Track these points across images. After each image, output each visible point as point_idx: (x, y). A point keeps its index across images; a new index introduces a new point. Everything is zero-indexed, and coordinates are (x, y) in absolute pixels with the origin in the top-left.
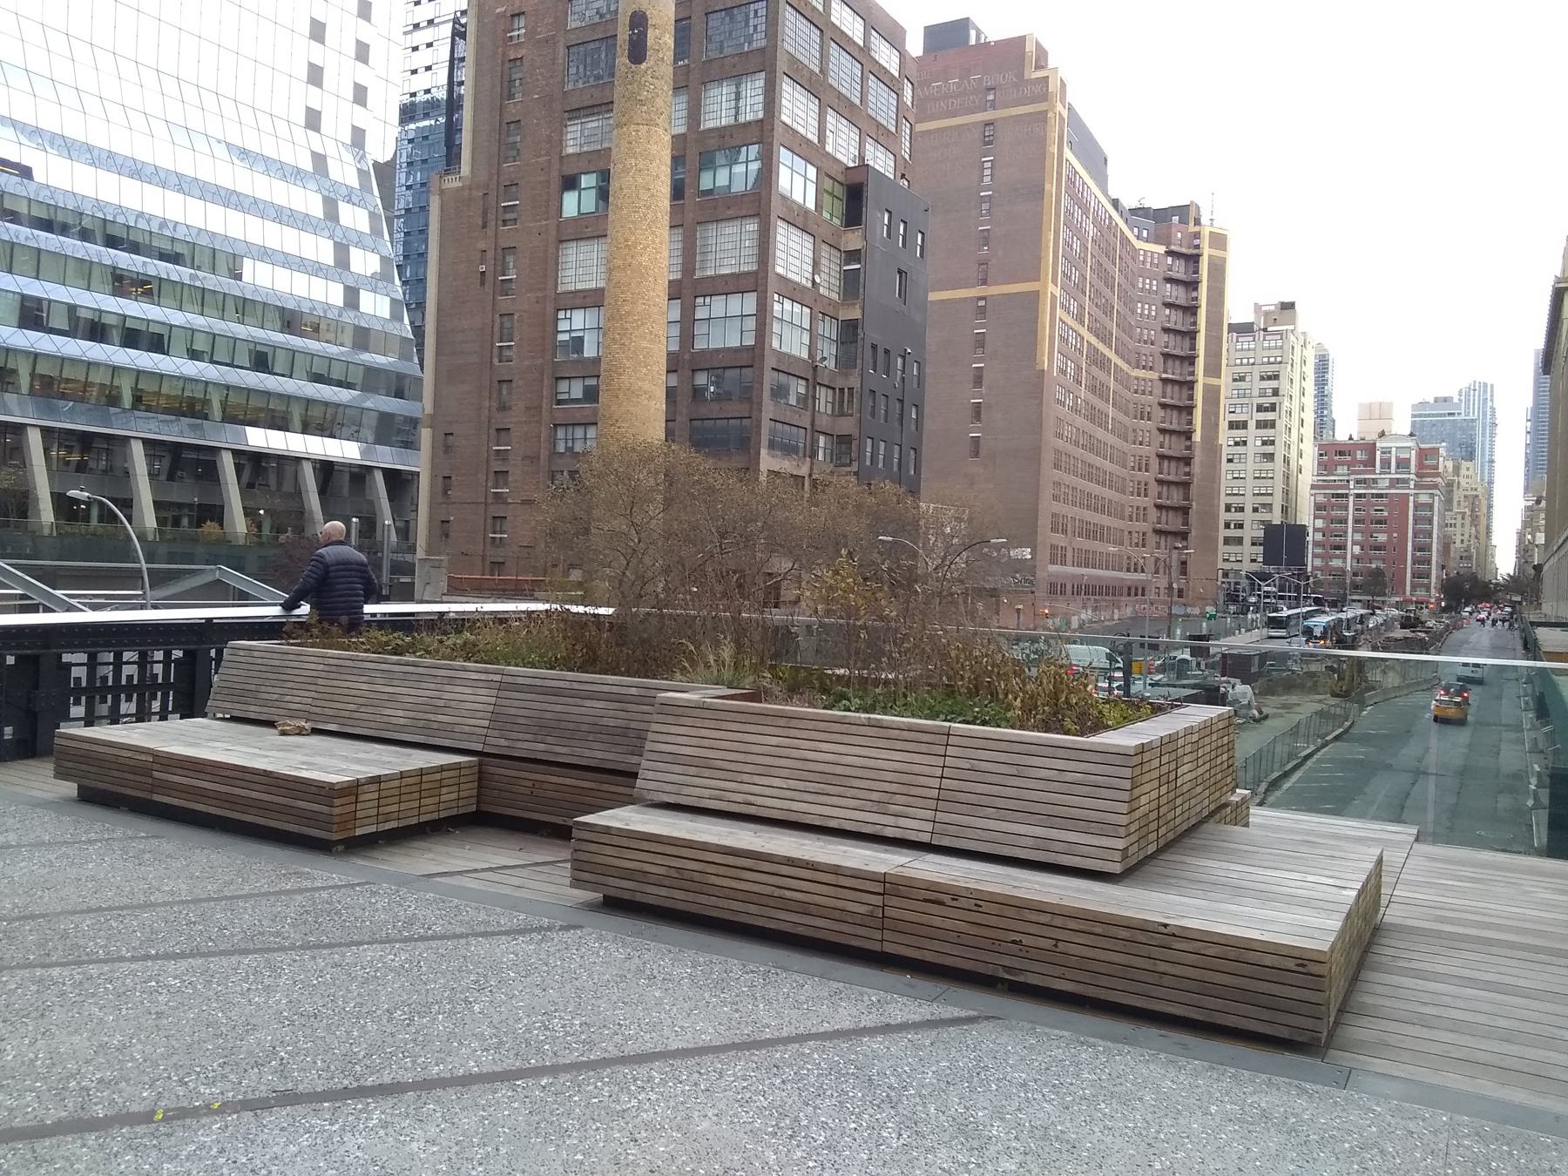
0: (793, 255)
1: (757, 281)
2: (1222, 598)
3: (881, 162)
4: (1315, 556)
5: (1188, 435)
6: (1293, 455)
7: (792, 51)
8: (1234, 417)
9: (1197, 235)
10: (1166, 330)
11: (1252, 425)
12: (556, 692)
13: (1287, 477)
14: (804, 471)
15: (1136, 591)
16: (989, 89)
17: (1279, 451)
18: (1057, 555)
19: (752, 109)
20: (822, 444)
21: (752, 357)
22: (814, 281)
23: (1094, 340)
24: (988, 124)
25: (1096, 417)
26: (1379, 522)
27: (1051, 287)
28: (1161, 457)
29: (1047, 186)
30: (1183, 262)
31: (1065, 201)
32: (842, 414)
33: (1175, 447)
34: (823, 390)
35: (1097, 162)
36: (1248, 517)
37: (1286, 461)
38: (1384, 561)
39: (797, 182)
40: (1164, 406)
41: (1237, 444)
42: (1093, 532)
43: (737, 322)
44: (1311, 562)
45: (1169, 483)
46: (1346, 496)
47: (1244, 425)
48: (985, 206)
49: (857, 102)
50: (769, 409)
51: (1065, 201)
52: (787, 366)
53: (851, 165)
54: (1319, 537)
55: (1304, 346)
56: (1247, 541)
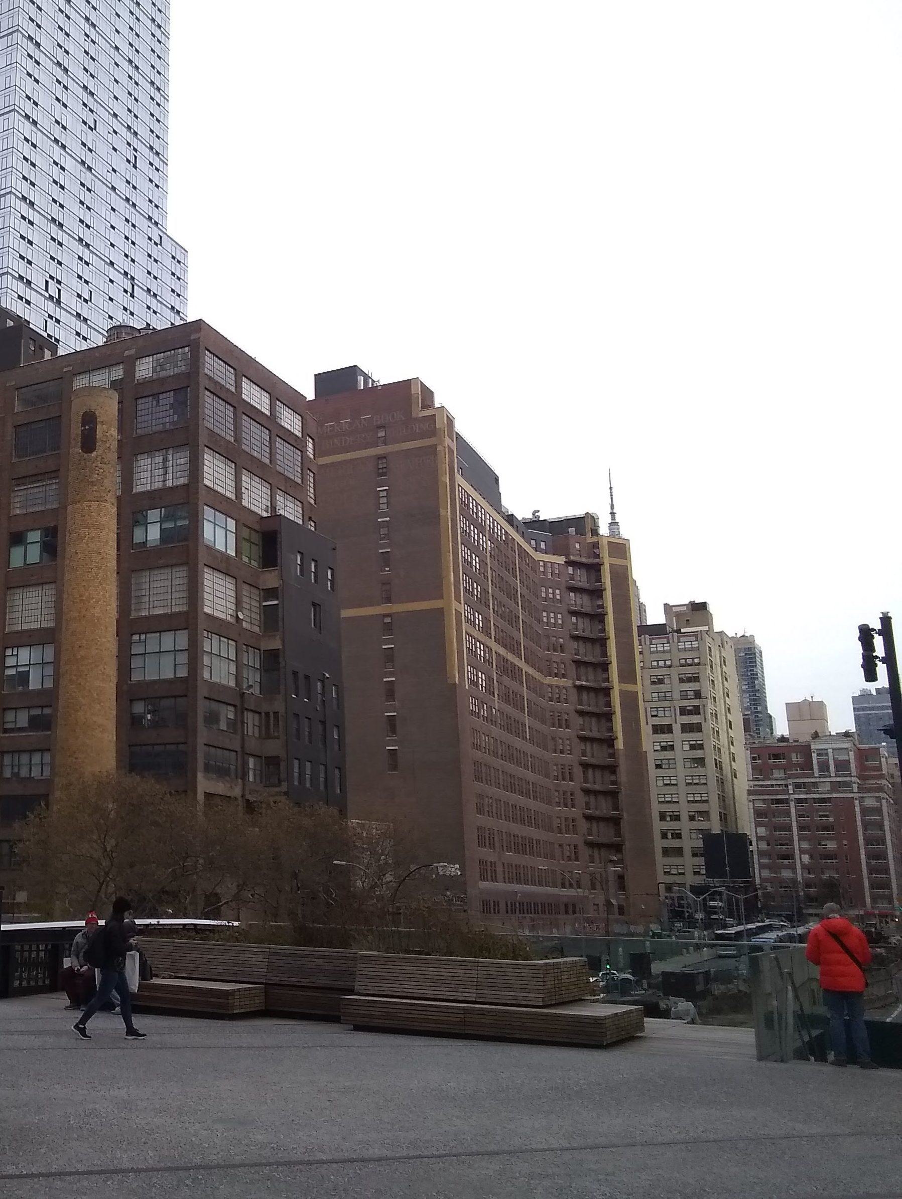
0: (218, 597)
1: (189, 620)
2: (665, 916)
3: (290, 510)
4: (762, 867)
5: (610, 742)
6: (725, 759)
7: (211, 426)
8: (657, 721)
9: (596, 545)
10: (576, 638)
11: (677, 728)
12: (300, 956)
13: (721, 782)
14: (237, 792)
15: (571, 908)
16: (379, 427)
17: (710, 756)
18: (487, 871)
19: (176, 478)
20: (251, 766)
21: (185, 687)
22: (237, 617)
23: (502, 651)
24: (380, 458)
25: (513, 726)
26: (826, 828)
27: (454, 605)
28: (585, 766)
29: (442, 512)
30: (584, 572)
31: (461, 522)
32: (268, 736)
33: (598, 755)
34: (250, 715)
35: (487, 481)
36: (685, 825)
37: (718, 765)
38: (837, 871)
39: (219, 534)
40: (581, 713)
41: (664, 748)
42: (523, 846)
43: (171, 657)
44: (759, 874)
45: (596, 793)
46: (786, 801)
47: (668, 729)
48: (383, 531)
49: (267, 461)
50: (203, 735)
51: (461, 522)
52: (217, 695)
53: (265, 514)
54: (763, 846)
55: (722, 646)
56: (687, 852)
